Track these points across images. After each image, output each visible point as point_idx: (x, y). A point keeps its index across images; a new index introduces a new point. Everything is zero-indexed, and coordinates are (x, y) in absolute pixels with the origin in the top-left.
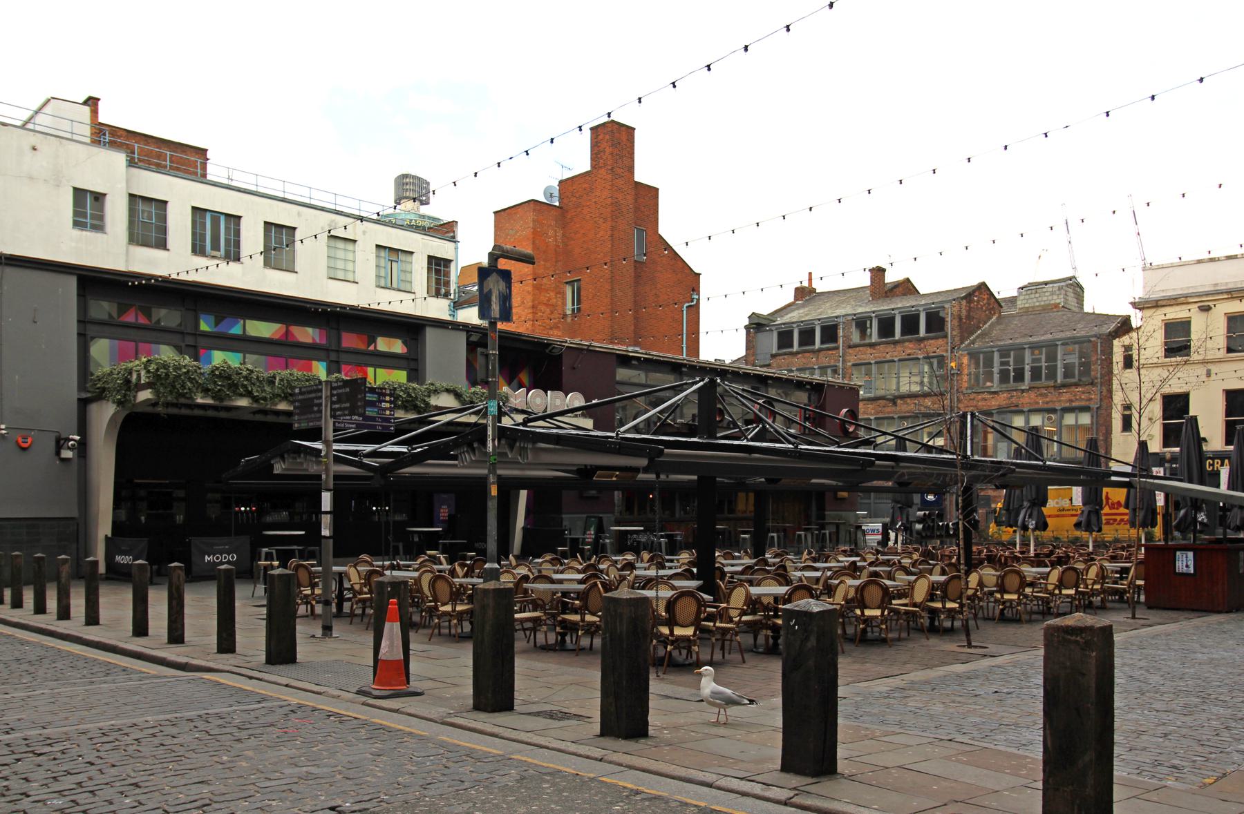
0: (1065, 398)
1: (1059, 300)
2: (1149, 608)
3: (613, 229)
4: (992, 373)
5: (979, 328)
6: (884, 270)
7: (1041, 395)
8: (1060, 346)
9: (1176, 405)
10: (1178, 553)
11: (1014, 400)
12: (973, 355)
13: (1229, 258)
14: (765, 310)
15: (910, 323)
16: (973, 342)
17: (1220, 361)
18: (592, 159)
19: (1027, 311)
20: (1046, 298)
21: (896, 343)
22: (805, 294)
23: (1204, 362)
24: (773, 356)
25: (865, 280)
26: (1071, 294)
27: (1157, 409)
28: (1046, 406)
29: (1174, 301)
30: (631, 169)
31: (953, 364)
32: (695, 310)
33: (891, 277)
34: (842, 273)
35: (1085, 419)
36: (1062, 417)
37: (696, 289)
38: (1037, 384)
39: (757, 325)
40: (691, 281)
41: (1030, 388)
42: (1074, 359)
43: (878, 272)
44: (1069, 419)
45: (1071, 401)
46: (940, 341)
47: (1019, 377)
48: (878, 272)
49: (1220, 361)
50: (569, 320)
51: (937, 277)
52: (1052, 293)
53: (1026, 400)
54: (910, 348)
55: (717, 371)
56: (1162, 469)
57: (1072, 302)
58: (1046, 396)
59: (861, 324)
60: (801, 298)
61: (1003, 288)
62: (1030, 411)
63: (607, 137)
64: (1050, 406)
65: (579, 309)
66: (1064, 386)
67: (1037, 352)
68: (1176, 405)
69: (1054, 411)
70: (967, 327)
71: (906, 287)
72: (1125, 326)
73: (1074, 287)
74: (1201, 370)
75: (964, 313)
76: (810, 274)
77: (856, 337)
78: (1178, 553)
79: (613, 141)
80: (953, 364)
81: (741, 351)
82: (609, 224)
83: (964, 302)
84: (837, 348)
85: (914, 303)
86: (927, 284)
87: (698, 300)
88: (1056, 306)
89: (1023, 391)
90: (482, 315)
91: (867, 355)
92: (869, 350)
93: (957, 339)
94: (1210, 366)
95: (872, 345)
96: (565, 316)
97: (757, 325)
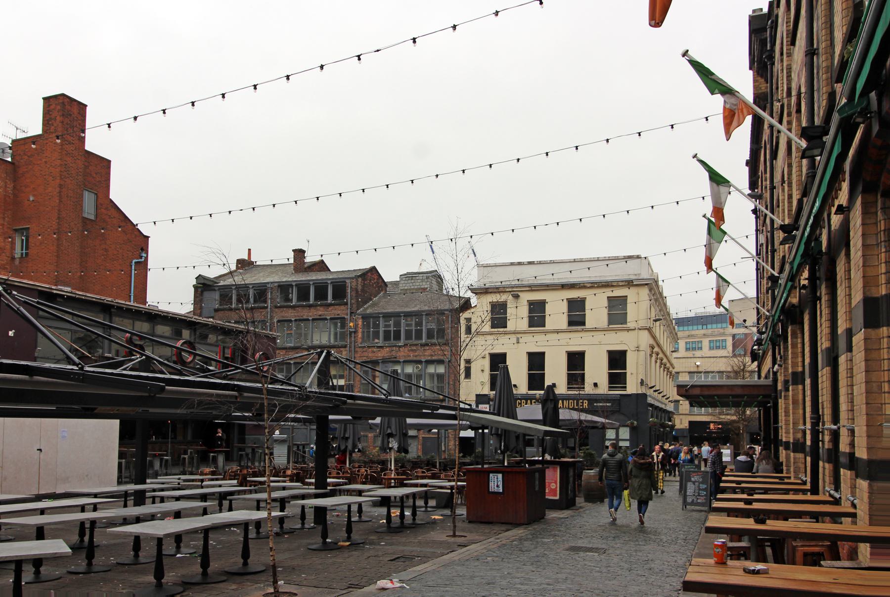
0: (426, 354)
1: (426, 285)
2: (470, 522)
3: (60, 186)
4: (378, 332)
5: (371, 299)
6: (304, 252)
7: (412, 350)
8: (429, 318)
9: (498, 361)
10: (491, 475)
11: (394, 353)
12: (365, 317)
13: (530, 263)
14: (212, 273)
15: (321, 290)
16: (367, 308)
17: (525, 333)
18: (43, 124)
19: (405, 292)
20: (418, 284)
21: (310, 306)
22: (244, 264)
23: (515, 333)
24: (216, 310)
25: (288, 257)
26: (434, 282)
27: (487, 363)
28: (415, 359)
29: (497, 290)
30: (82, 140)
31: (351, 324)
32: (143, 266)
33: (310, 258)
34: (273, 253)
35: (441, 369)
36: (426, 367)
37: (144, 248)
38: (410, 342)
39: (203, 286)
40: (139, 243)
41: (405, 345)
42: (433, 326)
43: (299, 254)
44: (431, 369)
45: (432, 355)
46: (343, 307)
47: (397, 337)
48: (299, 254)
49: (525, 333)
50: (17, 262)
51: (342, 262)
52: (422, 280)
53: (402, 354)
54: (320, 312)
55: (156, 317)
56: (488, 406)
57: (435, 287)
58: (414, 351)
59: (284, 288)
60: (242, 268)
61: (390, 275)
62: (404, 362)
63: (59, 107)
64: (418, 358)
65: (27, 254)
66: (427, 345)
67: (409, 319)
68: (498, 361)
69: (420, 362)
70: (364, 296)
71: (321, 266)
72: (466, 305)
73: (437, 277)
74: (513, 338)
75: (360, 287)
76: (249, 250)
77: (279, 301)
78: (491, 475)
79: (65, 114)
80: (351, 324)
81: (191, 308)
82: (58, 181)
83: (360, 280)
84: (267, 307)
85: (324, 277)
86: (336, 265)
87: (147, 258)
88: (425, 289)
89: (400, 347)
90: (684, 461)
91: (290, 314)
92: (291, 311)
93: (354, 306)
94: (519, 336)
95: (293, 307)
96: (13, 258)
97: (203, 286)
